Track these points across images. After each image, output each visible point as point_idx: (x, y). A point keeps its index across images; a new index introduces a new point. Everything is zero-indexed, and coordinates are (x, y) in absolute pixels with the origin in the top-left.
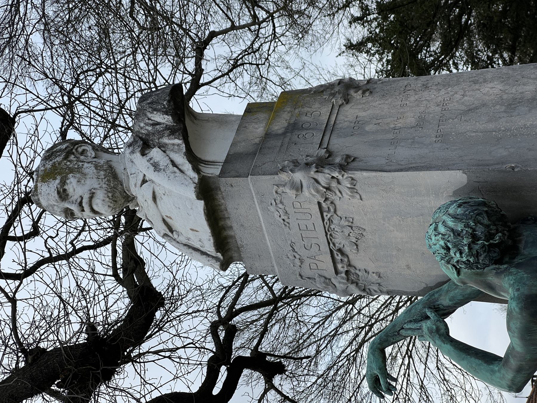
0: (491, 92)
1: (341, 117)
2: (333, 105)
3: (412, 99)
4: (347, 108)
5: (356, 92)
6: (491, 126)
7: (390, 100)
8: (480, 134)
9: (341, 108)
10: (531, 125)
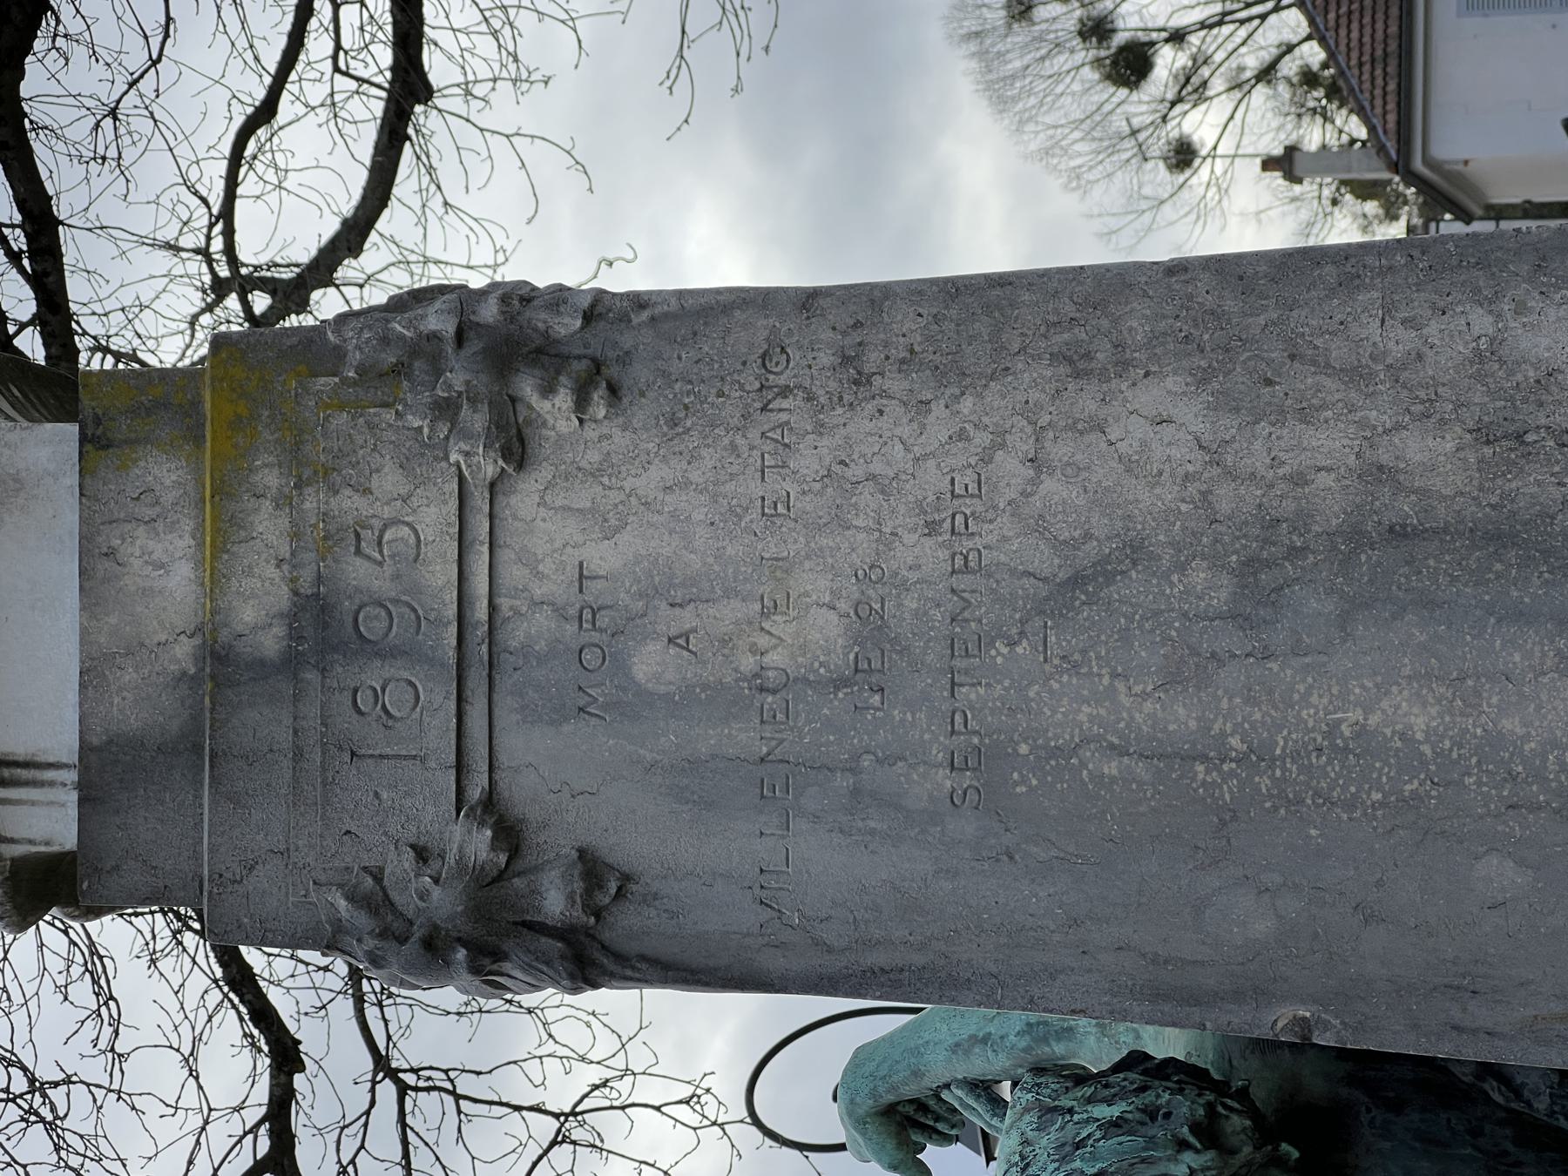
0: (1158, 452)
1: (513, 574)
2: (462, 480)
3: (809, 460)
4: (525, 497)
5: (548, 390)
6: (1182, 716)
7: (709, 457)
8: (1140, 768)
9: (501, 500)
10: (1361, 731)
